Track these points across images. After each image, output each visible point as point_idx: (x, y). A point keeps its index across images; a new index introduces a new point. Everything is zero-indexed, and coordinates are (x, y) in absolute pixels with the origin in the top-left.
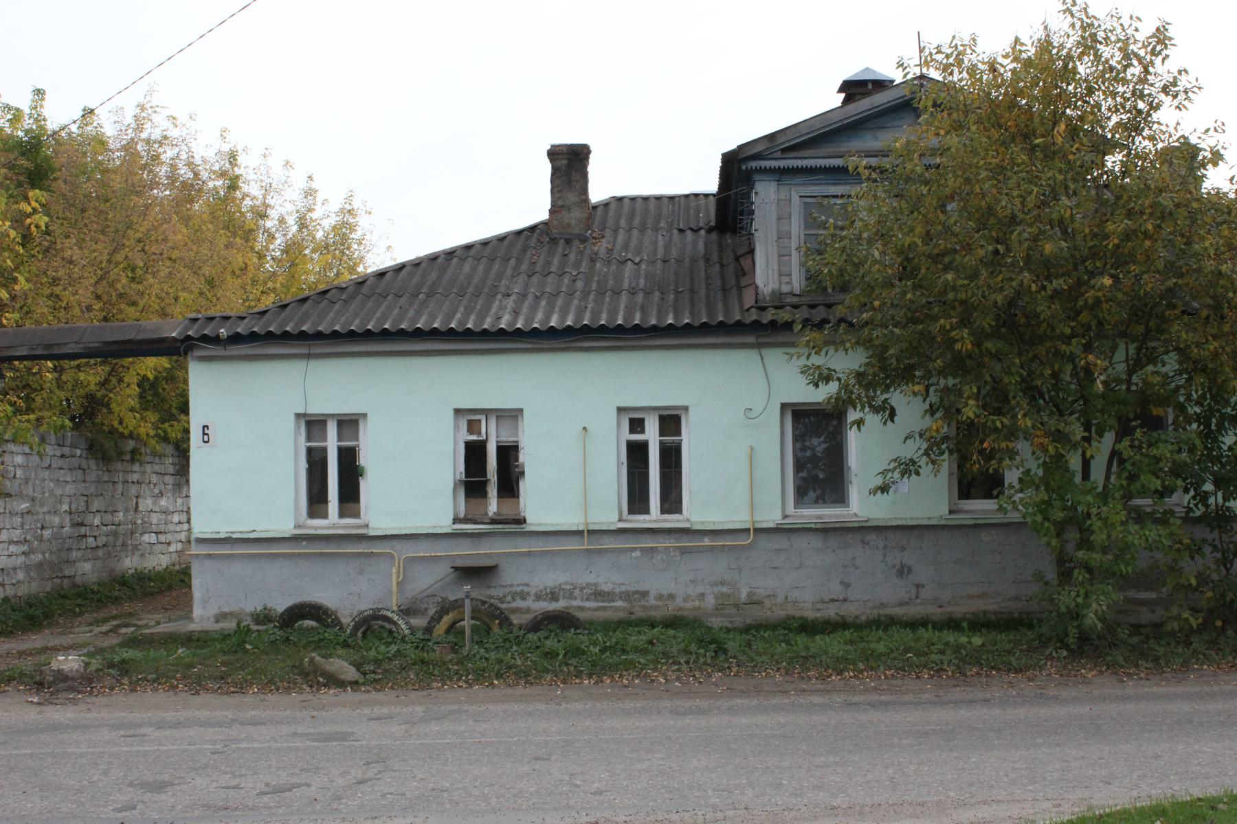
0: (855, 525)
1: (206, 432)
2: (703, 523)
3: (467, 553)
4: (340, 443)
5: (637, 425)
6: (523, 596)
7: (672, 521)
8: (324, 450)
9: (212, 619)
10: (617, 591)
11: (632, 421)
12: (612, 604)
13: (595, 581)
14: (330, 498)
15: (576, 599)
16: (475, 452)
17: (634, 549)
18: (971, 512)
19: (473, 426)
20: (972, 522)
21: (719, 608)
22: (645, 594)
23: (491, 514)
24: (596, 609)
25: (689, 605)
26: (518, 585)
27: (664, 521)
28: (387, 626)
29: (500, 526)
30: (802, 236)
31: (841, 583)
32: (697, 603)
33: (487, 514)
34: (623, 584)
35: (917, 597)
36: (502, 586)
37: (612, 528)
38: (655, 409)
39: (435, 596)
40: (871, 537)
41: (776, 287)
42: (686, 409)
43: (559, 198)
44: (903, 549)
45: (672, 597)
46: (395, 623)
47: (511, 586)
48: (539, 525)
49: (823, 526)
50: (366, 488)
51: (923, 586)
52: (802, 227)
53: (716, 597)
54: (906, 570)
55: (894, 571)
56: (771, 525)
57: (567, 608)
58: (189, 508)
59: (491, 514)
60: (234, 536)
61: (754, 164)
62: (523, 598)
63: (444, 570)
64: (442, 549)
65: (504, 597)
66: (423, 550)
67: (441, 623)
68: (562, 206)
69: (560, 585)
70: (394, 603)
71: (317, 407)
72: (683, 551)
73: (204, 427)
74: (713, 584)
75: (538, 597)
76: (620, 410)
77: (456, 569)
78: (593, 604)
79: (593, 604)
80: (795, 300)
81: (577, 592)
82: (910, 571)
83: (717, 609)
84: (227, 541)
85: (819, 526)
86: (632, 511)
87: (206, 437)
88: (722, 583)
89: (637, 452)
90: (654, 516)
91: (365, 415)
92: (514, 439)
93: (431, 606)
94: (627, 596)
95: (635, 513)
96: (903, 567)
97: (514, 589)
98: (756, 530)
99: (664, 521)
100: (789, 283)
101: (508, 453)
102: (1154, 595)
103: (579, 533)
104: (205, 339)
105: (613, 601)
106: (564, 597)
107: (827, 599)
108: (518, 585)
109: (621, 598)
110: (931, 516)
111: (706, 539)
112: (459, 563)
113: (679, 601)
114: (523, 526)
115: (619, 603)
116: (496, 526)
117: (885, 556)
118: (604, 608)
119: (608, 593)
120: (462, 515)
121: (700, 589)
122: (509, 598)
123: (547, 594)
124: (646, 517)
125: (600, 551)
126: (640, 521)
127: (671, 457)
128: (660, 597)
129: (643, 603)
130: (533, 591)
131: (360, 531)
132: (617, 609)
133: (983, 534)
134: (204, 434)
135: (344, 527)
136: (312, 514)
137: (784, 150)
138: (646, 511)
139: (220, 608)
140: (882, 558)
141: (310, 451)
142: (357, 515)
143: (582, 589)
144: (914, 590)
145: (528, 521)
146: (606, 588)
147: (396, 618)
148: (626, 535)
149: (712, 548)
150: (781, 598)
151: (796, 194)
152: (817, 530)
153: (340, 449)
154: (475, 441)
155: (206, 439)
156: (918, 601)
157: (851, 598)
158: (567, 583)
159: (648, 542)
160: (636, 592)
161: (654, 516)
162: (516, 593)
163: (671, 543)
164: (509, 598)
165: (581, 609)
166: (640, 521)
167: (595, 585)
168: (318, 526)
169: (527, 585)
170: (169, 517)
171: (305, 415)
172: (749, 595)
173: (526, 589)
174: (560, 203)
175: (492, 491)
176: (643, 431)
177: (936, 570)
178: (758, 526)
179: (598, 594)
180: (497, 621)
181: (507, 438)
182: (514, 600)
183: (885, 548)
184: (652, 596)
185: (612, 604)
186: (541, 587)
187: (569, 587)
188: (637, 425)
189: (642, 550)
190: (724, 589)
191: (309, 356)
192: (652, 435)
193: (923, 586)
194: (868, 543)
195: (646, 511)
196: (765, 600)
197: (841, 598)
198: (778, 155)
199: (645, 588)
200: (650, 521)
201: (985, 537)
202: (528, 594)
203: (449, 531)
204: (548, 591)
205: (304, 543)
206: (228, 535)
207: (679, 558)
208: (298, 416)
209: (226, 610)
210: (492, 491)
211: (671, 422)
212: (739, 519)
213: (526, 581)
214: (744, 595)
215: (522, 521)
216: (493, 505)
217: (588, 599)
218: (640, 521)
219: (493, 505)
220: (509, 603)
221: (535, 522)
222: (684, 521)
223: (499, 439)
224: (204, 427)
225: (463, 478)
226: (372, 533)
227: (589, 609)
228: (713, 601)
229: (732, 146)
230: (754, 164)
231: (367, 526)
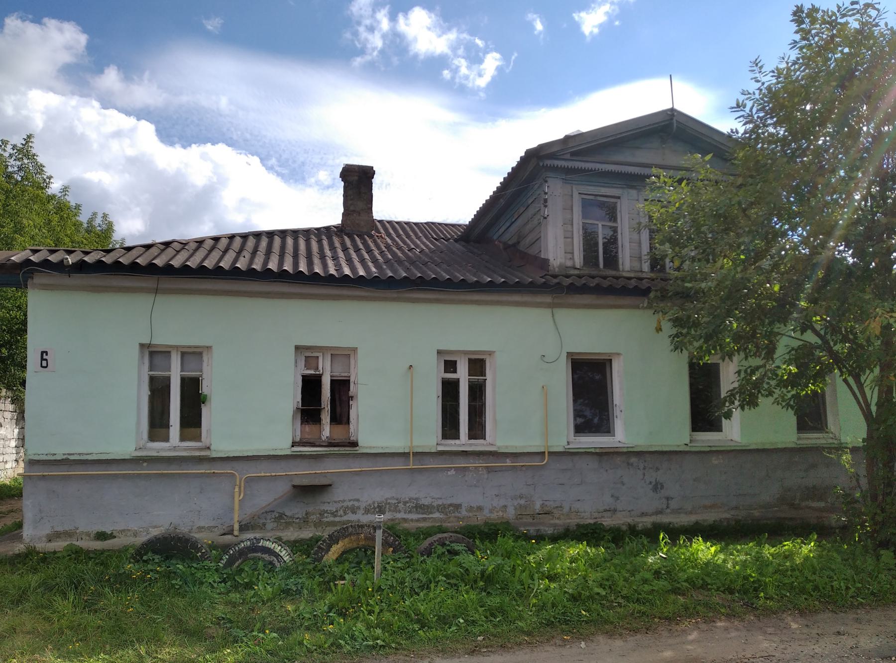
0: (625, 450)
1: (45, 357)
2: (507, 447)
3: (304, 473)
4: (182, 373)
5: (451, 366)
6: (354, 510)
7: (478, 445)
8: (168, 379)
9: (44, 539)
10: (435, 504)
11: (447, 363)
12: (431, 516)
13: (417, 496)
14: (172, 422)
15: (400, 512)
16: (311, 385)
17: (451, 468)
18: (703, 441)
19: (310, 361)
20: (708, 449)
21: (519, 516)
22: (458, 507)
23: (324, 438)
24: (418, 520)
25: (494, 516)
26: (350, 501)
27: (471, 445)
28: (266, 557)
29: (336, 449)
30: (581, 224)
31: (612, 496)
32: (501, 514)
33: (320, 438)
34: (441, 499)
35: (668, 507)
36: (335, 502)
37: (433, 450)
38: (465, 353)
39: (273, 511)
40: (633, 460)
41: (563, 261)
42: (490, 353)
43: (351, 205)
44: (658, 469)
45: (480, 509)
46: (277, 555)
47: (344, 501)
48: (370, 447)
49: (601, 451)
50: (208, 414)
51: (672, 498)
52: (581, 217)
53: (515, 509)
54: (659, 486)
55: (651, 486)
56: (561, 449)
57: (392, 520)
58: (24, 436)
59: (324, 438)
60: (72, 458)
61: (549, 162)
62: (354, 512)
63: (283, 488)
64: (280, 470)
65: (337, 511)
66: (263, 471)
67: (330, 553)
68: (354, 211)
69: (386, 500)
70: (236, 519)
71: (162, 339)
72: (489, 470)
73: (42, 353)
74: (514, 498)
75: (367, 511)
76: (439, 352)
77: (294, 486)
78: (414, 516)
79: (414, 516)
80: (576, 272)
81: (401, 505)
82: (662, 487)
83: (517, 518)
84: (65, 462)
85: (597, 451)
86: (445, 437)
87: (44, 364)
88: (521, 497)
89: (450, 389)
90: (463, 441)
91: (209, 348)
92: (346, 374)
93: (269, 521)
94: (442, 508)
95: (475, 438)
96: (657, 484)
97: (345, 504)
98: (550, 453)
99: (471, 445)
100: (572, 259)
101: (341, 387)
102: (822, 504)
103: (405, 455)
104: (46, 263)
105: (431, 513)
106: (390, 510)
107: (601, 509)
108: (350, 501)
109: (438, 510)
110: (679, 444)
111: (508, 460)
112: (297, 482)
113: (486, 512)
114: (357, 448)
115: (436, 515)
116: (332, 449)
117: (644, 474)
118: (424, 519)
119: (427, 506)
120: (298, 439)
121: (502, 502)
122: (341, 512)
123: (374, 508)
124: (457, 442)
125: (420, 471)
126: (452, 445)
127: (477, 392)
128: (471, 509)
129: (457, 514)
130: (363, 505)
131: (203, 453)
132: (434, 519)
133: (714, 458)
134: (42, 359)
135: (186, 449)
136: (152, 438)
137: (573, 154)
138: (457, 437)
139: (53, 527)
140: (642, 477)
141: (152, 379)
142: (198, 438)
143: (405, 503)
144: (665, 501)
145: (360, 444)
146: (426, 502)
147: (278, 549)
148: (444, 456)
149: (514, 468)
150: (566, 510)
151: (578, 191)
152: (596, 454)
153: (183, 380)
154: (311, 375)
155: (44, 364)
156: (668, 510)
157: (619, 508)
158: (393, 498)
159: (461, 463)
160: (451, 505)
161: (463, 441)
162: (347, 507)
163: (480, 463)
164: (341, 512)
165: (405, 520)
166: (452, 445)
167: (417, 499)
168: (158, 448)
169: (358, 500)
170: (7, 443)
171: (149, 345)
172: (542, 506)
173: (356, 504)
174: (352, 208)
175: (326, 417)
176: (455, 371)
177: (681, 486)
178: (551, 450)
179: (419, 508)
180: (392, 549)
181: (340, 374)
182: (345, 513)
183: (644, 469)
184: (464, 509)
185: (431, 516)
186: (370, 502)
187: (394, 501)
188: (451, 366)
189: (456, 469)
190: (522, 502)
191: (156, 291)
192: (462, 374)
193: (672, 498)
194: (632, 465)
195: (457, 437)
196: (555, 511)
197: (612, 508)
198: (568, 156)
199: (455, 501)
200: (460, 445)
201: (715, 461)
202: (359, 508)
203: (288, 452)
204: (376, 505)
205: (145, 464)
206: (64, 457)
207: (486, 476)
208: (142, 346)
209: (60, 529)
210: (326, 417)
211: (477, 365)
212: (534, 444)
213: (357, 497)
214: (538, 506)
215: (355, 444)
216: (326, 430)
217: (410, 512)
218: (451, 445)
219: (326, 430)
220: (341, 516)
221: (366, 445)
222: (487, 445)
223: (335, 374)
224: (42, 353)
225: (300, 407)
226: (214, 455)
227: (412, 520)
228: (513, 512)
229: (533, 144)
230: (549, 162)
231: (209, 448)
